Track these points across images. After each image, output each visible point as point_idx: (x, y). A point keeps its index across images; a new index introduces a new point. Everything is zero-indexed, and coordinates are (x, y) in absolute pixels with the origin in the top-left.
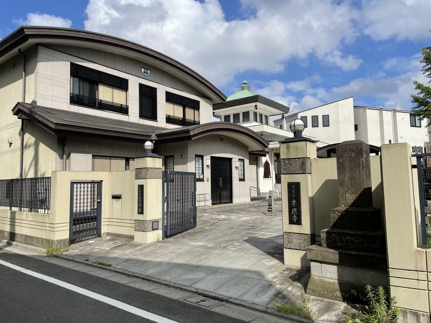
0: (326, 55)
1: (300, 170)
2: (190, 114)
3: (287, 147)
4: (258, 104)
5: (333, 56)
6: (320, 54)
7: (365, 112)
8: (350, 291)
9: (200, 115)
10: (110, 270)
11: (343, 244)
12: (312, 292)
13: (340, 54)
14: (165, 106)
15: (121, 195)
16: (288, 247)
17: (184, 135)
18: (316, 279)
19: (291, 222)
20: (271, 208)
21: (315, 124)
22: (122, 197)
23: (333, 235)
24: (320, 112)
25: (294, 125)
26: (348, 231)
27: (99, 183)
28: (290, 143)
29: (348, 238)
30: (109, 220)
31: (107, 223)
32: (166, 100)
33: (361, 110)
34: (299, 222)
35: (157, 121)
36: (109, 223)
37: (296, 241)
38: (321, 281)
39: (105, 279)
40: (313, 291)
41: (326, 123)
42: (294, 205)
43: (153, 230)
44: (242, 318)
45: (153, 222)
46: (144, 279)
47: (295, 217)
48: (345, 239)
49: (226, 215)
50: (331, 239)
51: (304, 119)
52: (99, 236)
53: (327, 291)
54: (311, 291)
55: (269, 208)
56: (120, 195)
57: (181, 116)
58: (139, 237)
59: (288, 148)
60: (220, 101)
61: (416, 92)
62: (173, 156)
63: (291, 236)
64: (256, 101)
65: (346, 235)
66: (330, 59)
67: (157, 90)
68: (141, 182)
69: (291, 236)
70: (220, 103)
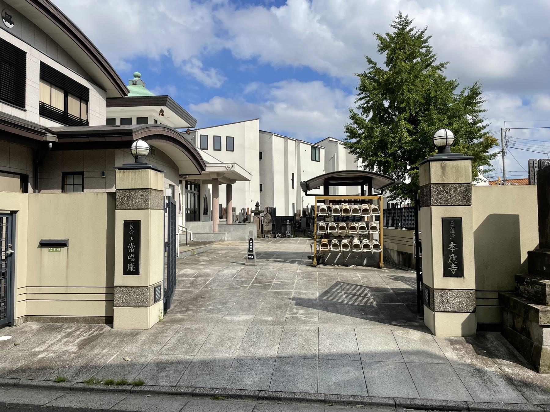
0: (184, 62)
1: (462, 200)
2: (75, 108)
3: (441, 166)
4: (165, 108)
5: (193, 65)
6: (177, 60)
7: (271, 138)
9: (90, 112)
10: (145, 393)
13: (201, 65)
14: (38, 87)
16: (442, 309)
17: (119, 139)
20: (253, 255)
21: (217, 148)
22: (70, 244)
24: (224, 131)
25: (136, 147)
27: (10, 217)
28: (446, 162)
30: (30, 290)
31: (24, 297)
32: (40, 78)
33: (267, 136)
34: (459, 273)
35: (25, 111)
36: (30, 296)
37: (454, 301)
41: (230, 148)
42: (452, 250)
43: (155, 302)
45: (155, 288)
47: (131, 267)
51: (204, 138)
52: (10, 323)
54: (546, 368)
55: (249, 255)
57: (62, 108)
59: (443, 168)
60: (118, 95)
61: (457, 83)
62: (82, 174)
63: (446, 294)
64: (164, 104)
66: (188, 68)
67: (27, 55)
69: (446, 294)
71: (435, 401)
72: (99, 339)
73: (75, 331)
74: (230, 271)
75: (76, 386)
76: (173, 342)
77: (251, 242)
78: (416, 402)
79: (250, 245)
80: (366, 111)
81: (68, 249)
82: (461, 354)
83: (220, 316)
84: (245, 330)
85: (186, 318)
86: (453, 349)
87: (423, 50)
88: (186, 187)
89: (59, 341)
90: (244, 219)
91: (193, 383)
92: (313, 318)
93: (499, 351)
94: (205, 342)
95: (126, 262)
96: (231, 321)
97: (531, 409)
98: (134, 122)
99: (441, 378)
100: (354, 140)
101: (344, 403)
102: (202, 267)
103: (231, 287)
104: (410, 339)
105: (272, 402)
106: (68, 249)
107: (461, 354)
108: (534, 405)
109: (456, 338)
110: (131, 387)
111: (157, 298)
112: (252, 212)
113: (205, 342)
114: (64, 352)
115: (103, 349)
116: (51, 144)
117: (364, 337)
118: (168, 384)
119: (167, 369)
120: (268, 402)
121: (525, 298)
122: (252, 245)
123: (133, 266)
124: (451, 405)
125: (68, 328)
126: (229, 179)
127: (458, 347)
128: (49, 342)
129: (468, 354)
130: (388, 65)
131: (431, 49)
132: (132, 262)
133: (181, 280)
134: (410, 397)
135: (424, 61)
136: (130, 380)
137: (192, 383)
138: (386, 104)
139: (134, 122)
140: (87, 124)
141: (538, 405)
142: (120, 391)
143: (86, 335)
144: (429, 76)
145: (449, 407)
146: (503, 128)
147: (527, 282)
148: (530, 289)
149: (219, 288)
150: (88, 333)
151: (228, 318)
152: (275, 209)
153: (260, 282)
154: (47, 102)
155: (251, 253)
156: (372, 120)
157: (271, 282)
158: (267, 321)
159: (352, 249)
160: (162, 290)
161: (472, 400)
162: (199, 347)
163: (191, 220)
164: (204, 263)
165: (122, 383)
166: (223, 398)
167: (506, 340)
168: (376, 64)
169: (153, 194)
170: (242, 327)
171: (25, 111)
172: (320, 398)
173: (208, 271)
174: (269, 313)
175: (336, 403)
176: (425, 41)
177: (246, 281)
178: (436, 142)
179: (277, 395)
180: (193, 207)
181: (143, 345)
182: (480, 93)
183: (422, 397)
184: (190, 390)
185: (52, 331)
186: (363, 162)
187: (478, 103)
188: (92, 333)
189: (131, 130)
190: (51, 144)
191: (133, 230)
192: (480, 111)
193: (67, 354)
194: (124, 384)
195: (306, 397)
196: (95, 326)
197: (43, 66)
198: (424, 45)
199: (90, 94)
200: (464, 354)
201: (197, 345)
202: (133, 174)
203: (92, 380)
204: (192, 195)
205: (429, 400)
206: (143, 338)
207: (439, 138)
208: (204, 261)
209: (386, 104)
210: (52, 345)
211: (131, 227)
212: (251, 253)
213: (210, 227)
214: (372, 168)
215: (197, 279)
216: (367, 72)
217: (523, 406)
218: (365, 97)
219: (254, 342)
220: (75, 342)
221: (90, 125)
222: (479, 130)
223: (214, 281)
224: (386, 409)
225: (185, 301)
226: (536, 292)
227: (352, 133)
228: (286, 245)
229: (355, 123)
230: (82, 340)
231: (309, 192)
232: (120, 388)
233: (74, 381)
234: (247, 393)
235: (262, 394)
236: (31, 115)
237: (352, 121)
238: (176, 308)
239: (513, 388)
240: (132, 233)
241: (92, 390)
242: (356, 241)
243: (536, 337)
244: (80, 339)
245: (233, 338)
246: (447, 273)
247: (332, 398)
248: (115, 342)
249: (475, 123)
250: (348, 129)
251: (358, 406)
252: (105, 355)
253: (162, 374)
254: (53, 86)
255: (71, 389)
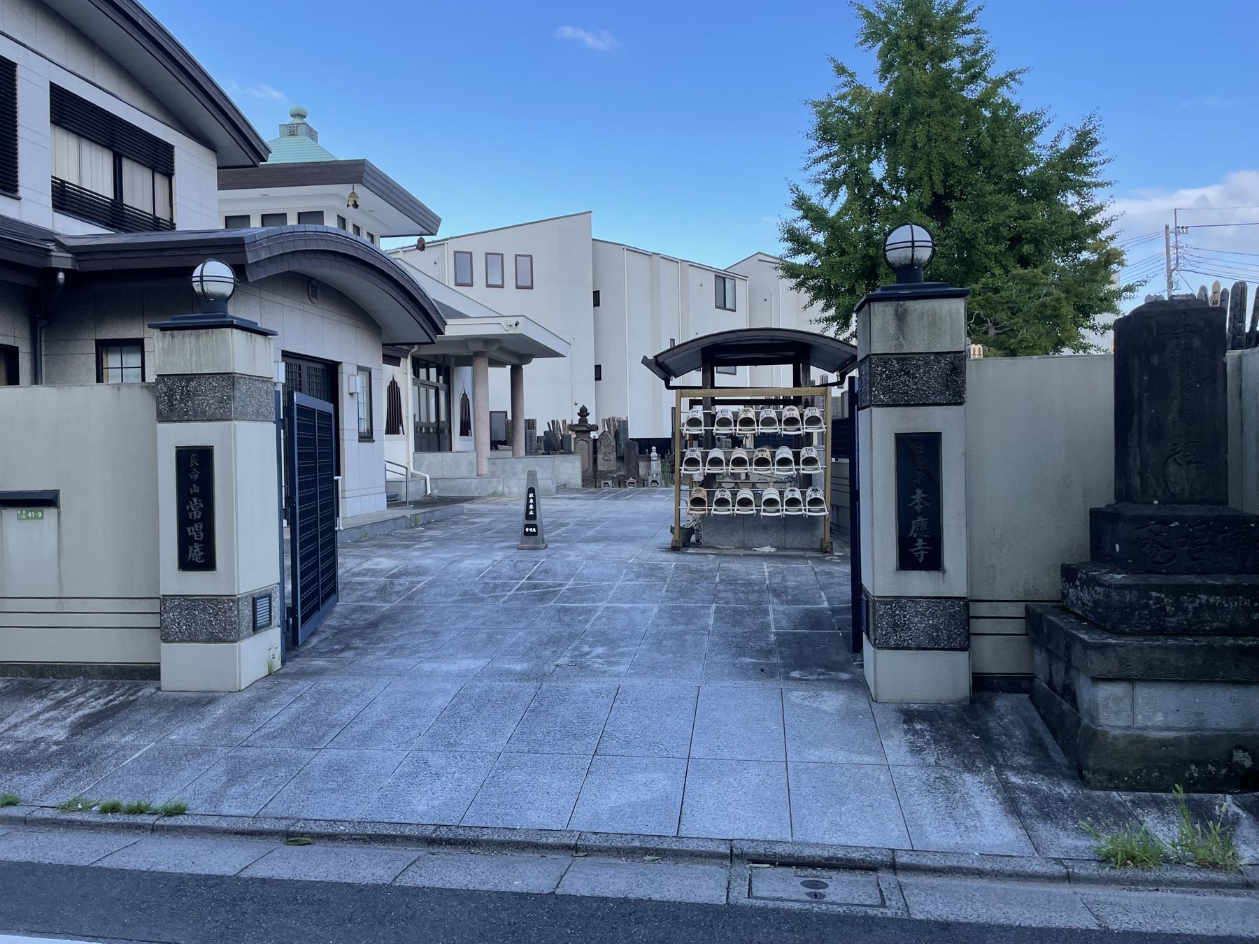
1: (942, 393)
2: (140, 190)
4: (360, 190)
8: (1231, 755)
11: (1187, 620)
12: (1109, 781)
15: (56, 494)
18: (1116, 738)
19: (186, 564)
20: (535, 526)
23: (1154, 594)
25: (201, 277)
26: (1197, 580)
29: (1204, 597)
35: (19, 199)
38: (1132, 742)
39: (404, 890)
40: (1111, 775)
42: (919, 507)
43: (256, 629)
44: (1060, 920)
45: (254, 600)
46: (432, 842)
47: (196, 553)
48: (1193, 602)
49: (389, 556)
50: (1148, 605)
53: (1159, 769)
54: (1103, 778)
55: (529, 526)
56: (51, 492)
57: (109, 193)
58: (184, 665)
59: (901, 318)
61: (1045, 119)
65: (1194, 590)
68: (194, 434)
70: (243, 159)
71: (824, 847)
72: (122, 715)
73: (77, 695)
74: (478, 561)
75: (38, 814)
76: (284, 718)
77: (531, 495)
78: (779, 849)
79: (528, 504)
80: (832, 187)
81: (59, 514)
82: (920, 743)
83: (411, 662)
84: (453, 694)
85: (334, 666)
86: (906, 732)
87: (966, 41)
88: (416, 373)
89: (33, 718)
90: (553, 444)
91: (296, 810)
92: (618, 663)
93: (1010, 736)
94: (353, 721)
95: (184, 542)
96: (431, 674)
97: (1037, 868)
98: (255, 223)
99: (854, 796)
100: (801, 260)
101: (619, 852)
102: (417, 554)
103: (468, 597)
104: (817, 710)
105: (460, 850)
106: (59, 514)
107: (920, 743)
108: (1048, 860)
109: (922, 708)
110: (155, 817)
111: (262, 619)
112: (571, 427)
113: (353, 721)
114: (37, 742)
115: (124, 736)
116: (61, 276)
117: (713, 706)
118: (241, 812)
119: (249, 779)
120: (451, 851)
121: (1076, 614)
122: (534, 504)
123: (198, 548)
124: (856, 855)
125: (62, 689)
126: (516, 353)
127: (918, 727)
128: (13, 720)
129: (937, 742)
130: (883, 77)
131: (986, 37)
132: (198, 542)
133: (360, 584)
134: (770, 837)
135: (967, 67)
136: (158, 803)
137: (294, 810)
138: (878, 170)
139: (255, 223)
140: (172, 226)
141: (1058, 861)
142: (130, 827)
143: (97, 705)
144: (982, 102)
145: (849, 860)
146: (1172, 227)
147: (1080, 579)
148: (1086, 597)
149: (439, 599)
150: (102, 701)
151: (427, 667)
152: (625, 423)
153: (536, 587)
154: (71, 178)
155: (532, 522)
156: (845, 209)
157: (561, 585)
158: (509, 673)
159: (758, 511)
160: (276, 604)
161: (907, 846)
162: (337, 730)
163: (429, 449)
164: (428, 544)
165: (139, 810)
166: (310, 840)
167: (1035, 713)
168: (851, 75)
169: (242, 387)
170: (449, 686)
171: (19, 199)
172: (566, 841)
173: (427, 562)
174: (525, 656)
175: (600, 851)
176: (969, 19)
177: (504, 585)
178: (892, 256)
179: (472, 835)
180: (433, 419)
181: (216, 725)
182: (1095, 143)
183: (797, 838)
184: (282, 826)
185: (26, 695)
186: (823, 310)
187: (1091, 165)
188: (111, 701)
189: (242, 239)
190: (61, 276)
191: (196, 470)
192: (1096, 185)
193: (42, 746)
194: (142, 812)
195: (535, 839)
196: (124, 685)
197: (56, 91)
198: (967, 27)
199: (176, 158)
200: (928, 743)
201: (333, 726)
202: (193, 339)
203: (76, 801)
204: (432, 392)
205: (808, 845)
206: (221, 711)
207: (899, 246)
208: (431, 539)
209: (878, 170)
210: (16, 726)
211: (194, 462)
212: (532, 522)
213: (471, 463)
214: (845, 324)
215: (396, 581)
216: (835, 94)
217: (1022, 861)
218: (827, 156)
219: (464, 719)
220: (69, 720)
221: (178, 228)
222: (1096, 229)
223: (432, 584)
224: (710, 864)
225: (350, 629)
226: (1094, 602)
227: (799, 242)
228: (635, 503)
229: (805, 217)
230: (84, 716)
231: (674, 382)
232: (132, 819)
233: (36, 803)
234: (407, 831)
235: (443, 833)
236: (32, 207)
237: (800, 213)
238: (323, 645)
239: (1014, 820)
240: (196, 477)
241: (70, 825)
242: (771, 493)
243: (1085, 706)
244: (80, 713)
245: (419, 710)
246: (907, 561)
247: (593, 841)
248: (154, 721)
249: (1087, 214)
250: (788, 231)
251: (648, 858)
252: (123, 748)
253: (235, 790)
254: (84, 140)
255: (27, 822)
